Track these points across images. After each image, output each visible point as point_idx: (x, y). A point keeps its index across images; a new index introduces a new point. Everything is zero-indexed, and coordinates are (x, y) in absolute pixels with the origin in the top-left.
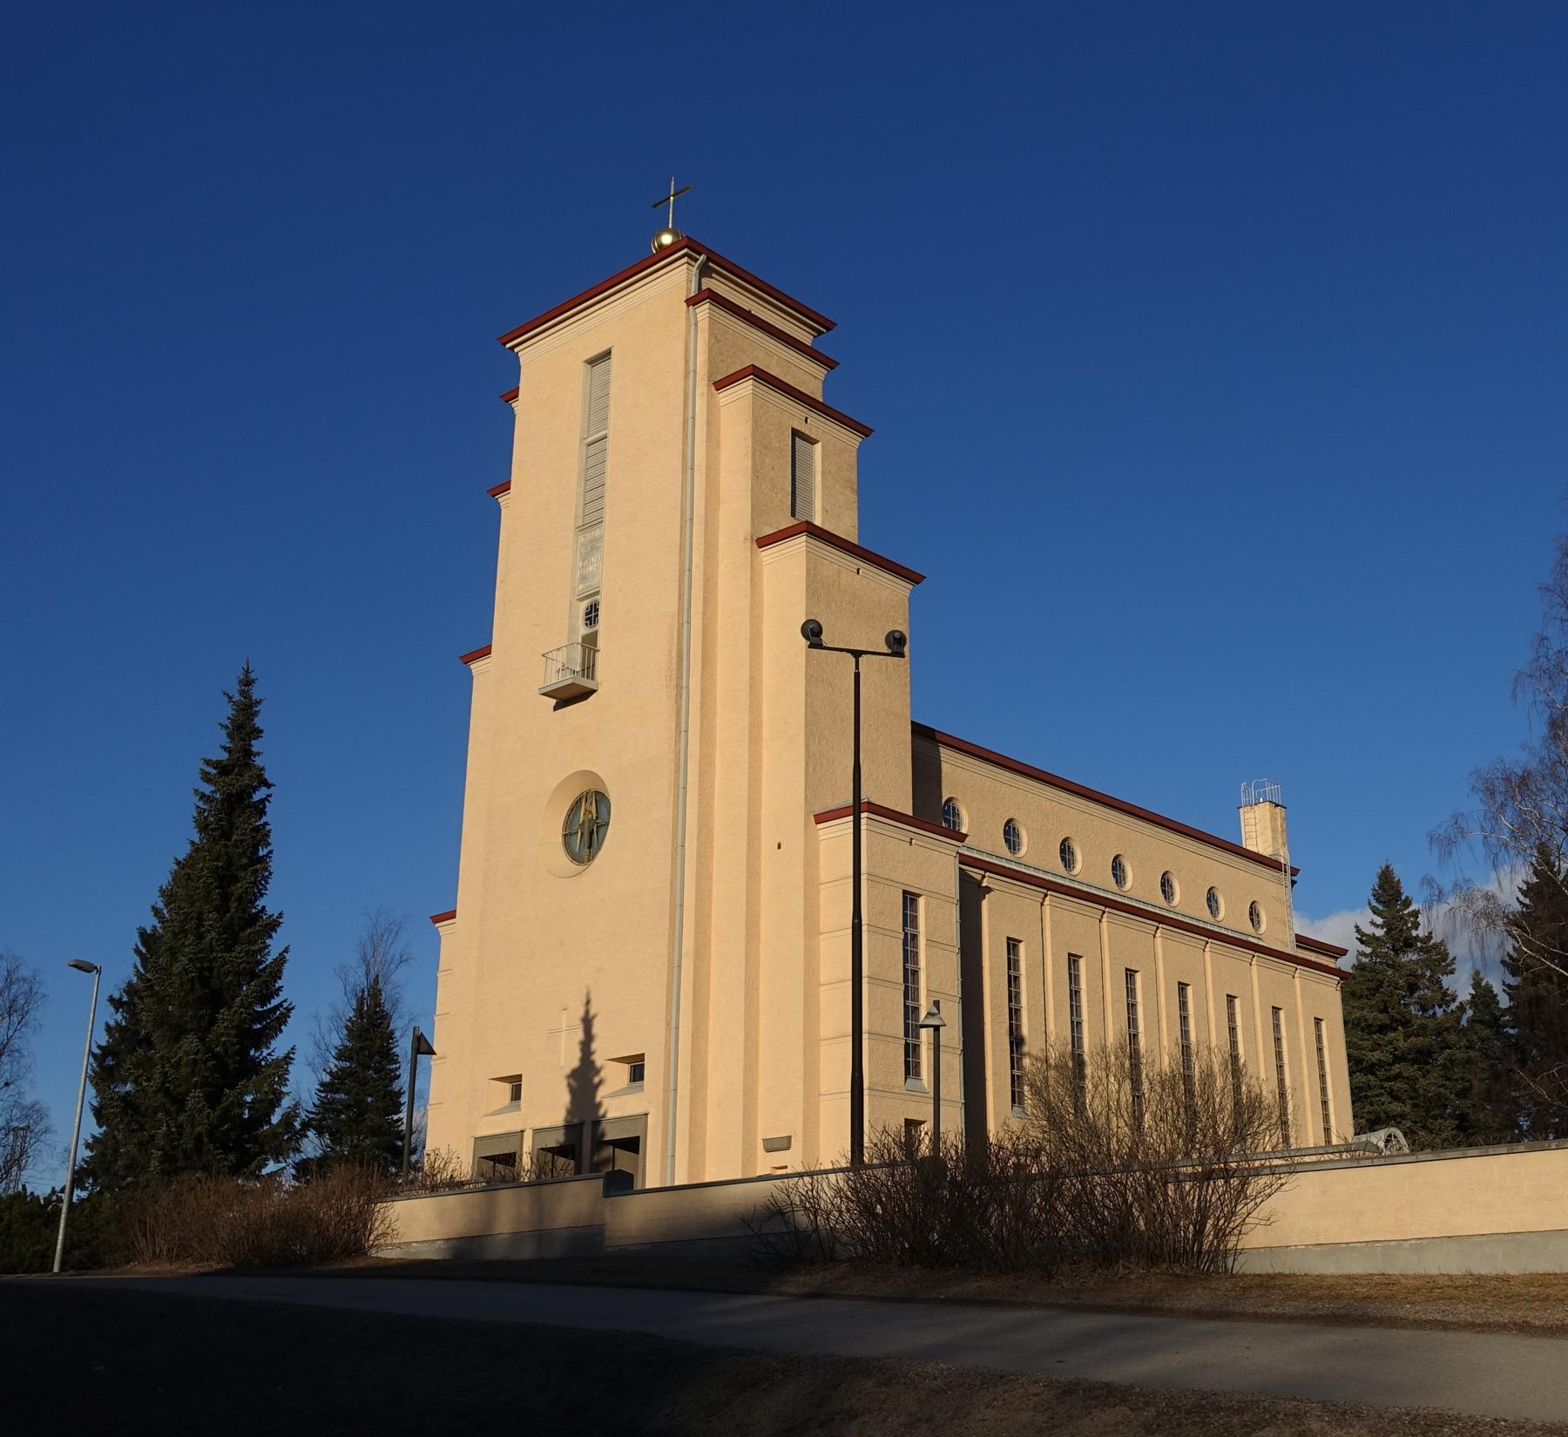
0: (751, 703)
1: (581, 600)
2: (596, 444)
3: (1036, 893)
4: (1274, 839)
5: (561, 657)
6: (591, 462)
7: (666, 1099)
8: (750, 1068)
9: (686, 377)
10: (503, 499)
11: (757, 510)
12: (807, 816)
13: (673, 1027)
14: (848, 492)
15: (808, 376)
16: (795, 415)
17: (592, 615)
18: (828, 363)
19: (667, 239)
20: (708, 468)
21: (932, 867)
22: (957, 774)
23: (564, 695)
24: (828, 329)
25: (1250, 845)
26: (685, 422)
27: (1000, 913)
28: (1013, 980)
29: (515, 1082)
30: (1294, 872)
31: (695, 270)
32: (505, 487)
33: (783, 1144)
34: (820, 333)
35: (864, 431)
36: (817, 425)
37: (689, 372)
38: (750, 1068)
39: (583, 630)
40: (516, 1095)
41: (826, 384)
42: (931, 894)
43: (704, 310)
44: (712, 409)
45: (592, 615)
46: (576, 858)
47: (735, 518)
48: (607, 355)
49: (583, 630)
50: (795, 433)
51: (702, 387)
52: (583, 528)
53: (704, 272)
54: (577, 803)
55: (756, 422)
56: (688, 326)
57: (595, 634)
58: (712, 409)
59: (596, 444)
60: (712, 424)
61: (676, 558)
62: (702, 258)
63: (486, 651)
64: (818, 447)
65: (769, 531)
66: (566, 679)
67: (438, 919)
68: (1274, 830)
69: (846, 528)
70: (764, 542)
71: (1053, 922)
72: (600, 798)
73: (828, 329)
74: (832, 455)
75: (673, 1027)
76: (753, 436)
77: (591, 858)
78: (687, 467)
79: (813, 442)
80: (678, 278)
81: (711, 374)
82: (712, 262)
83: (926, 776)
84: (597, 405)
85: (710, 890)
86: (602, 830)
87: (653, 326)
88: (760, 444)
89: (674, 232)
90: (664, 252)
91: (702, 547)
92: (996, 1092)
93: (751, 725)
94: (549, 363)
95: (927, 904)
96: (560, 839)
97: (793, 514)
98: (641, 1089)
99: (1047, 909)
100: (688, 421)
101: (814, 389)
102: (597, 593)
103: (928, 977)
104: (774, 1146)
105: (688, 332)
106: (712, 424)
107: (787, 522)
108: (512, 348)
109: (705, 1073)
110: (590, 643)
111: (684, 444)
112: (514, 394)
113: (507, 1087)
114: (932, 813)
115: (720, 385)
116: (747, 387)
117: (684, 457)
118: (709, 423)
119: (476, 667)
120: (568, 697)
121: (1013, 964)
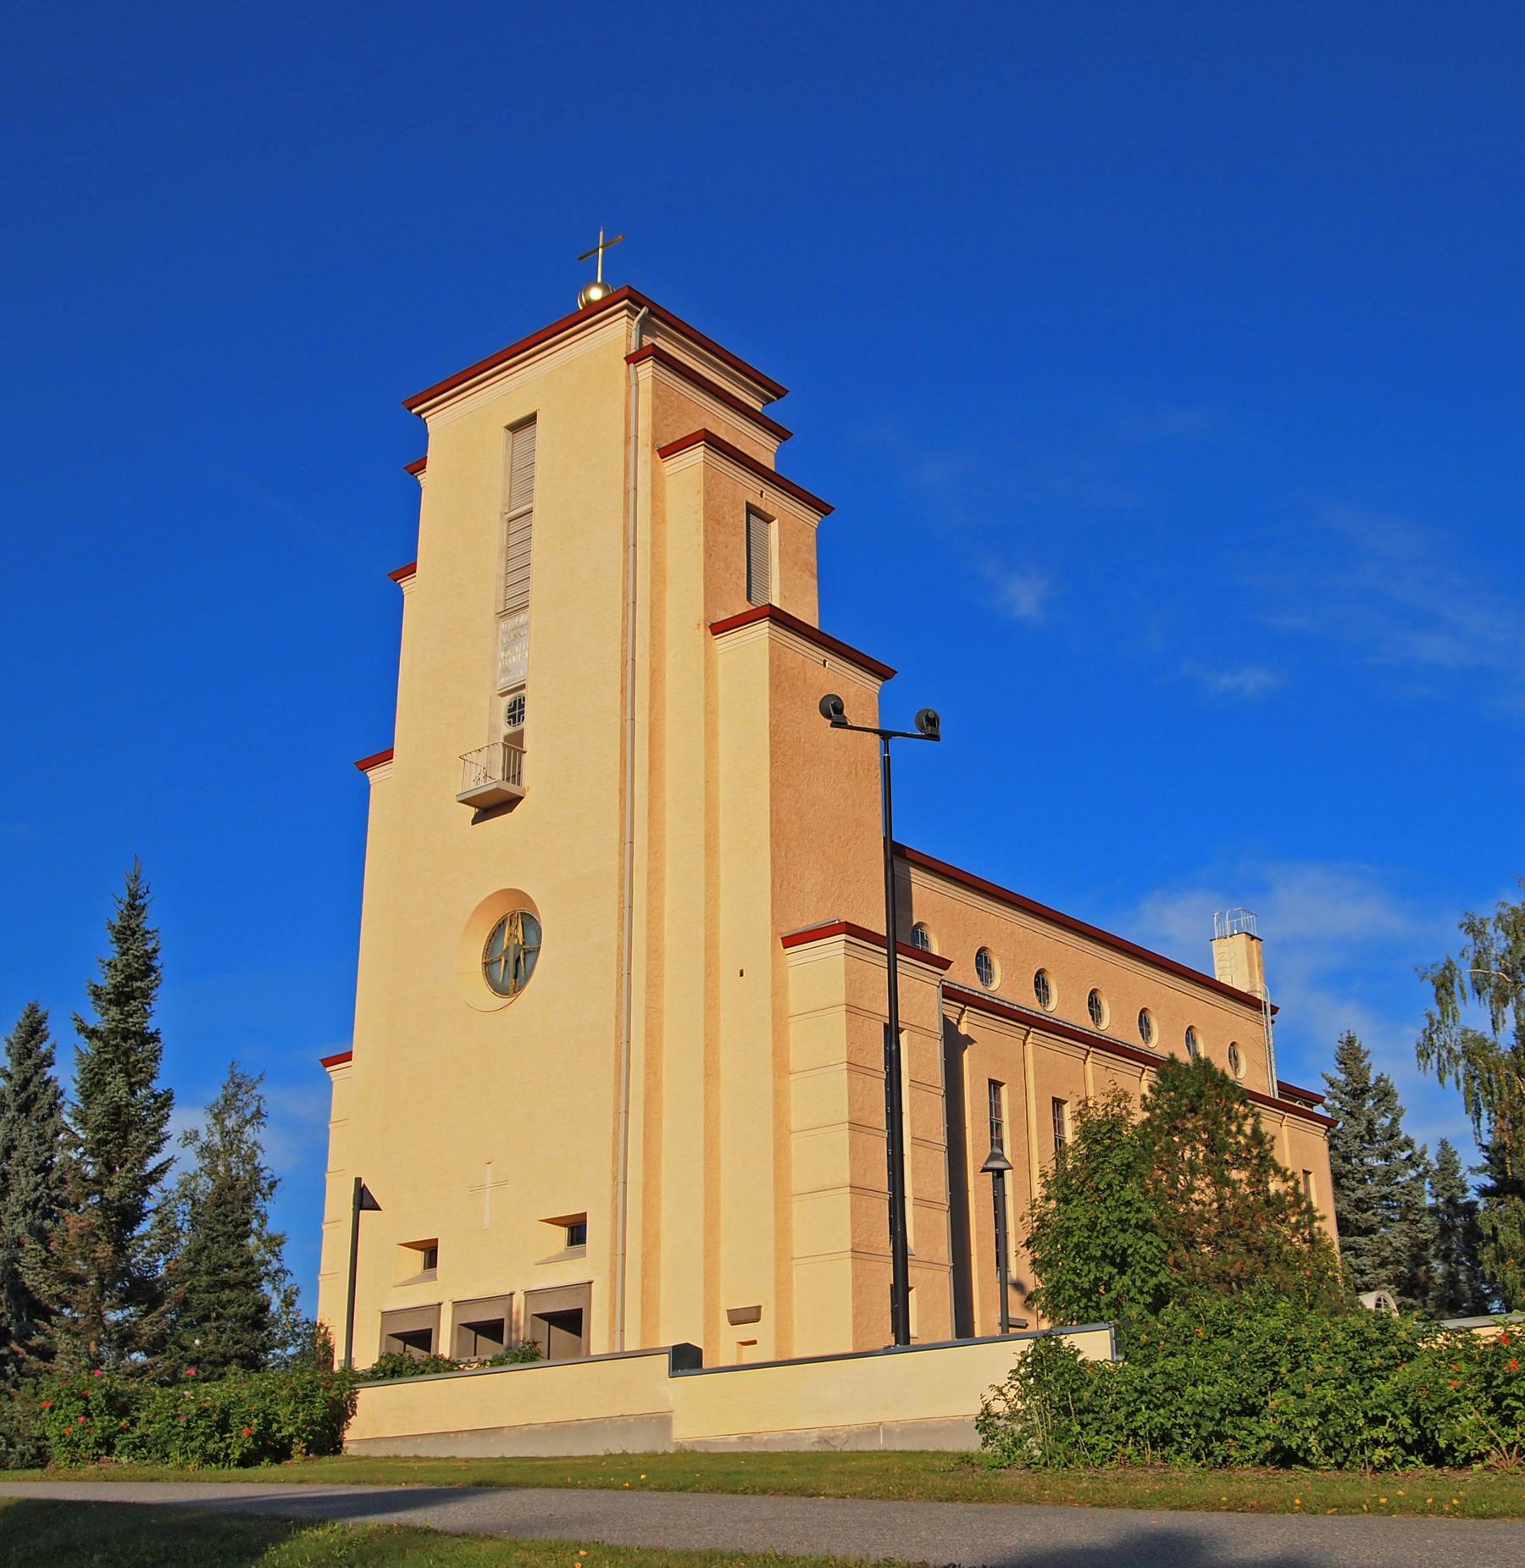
0: (707, 810)
1: (503, 695)
2: (519, 519)
3: (1018, 1030)
4: (1251, 974)
5: (482, 759)
6: (514, 539)
7: (613, 1264)
8: (711, 1228)
9: (627, 443)
10: (407, 585)
11: (712, 591)
12: (774, 936)
13: (621, 1181)
14: (806, 576)
15: (763, 448)
16: (752, 490)
17: (516, 712)
18: (781, 433)
19: (596, 294)
20: (654, 545)
21: (921, 997)
22: (924, 889)
23: (488, 802)
24: (779, 397)
25: (1222, 976)
26: (626, 493)
27: (991, 1048)
28: (996, 1127)
29: (430, 1251)
30: (1274, 1010)
31: (635, 323)
32: (410, 569)
33: (751, 1315)
34: (769, 401)
35: (823, 508)
36: (773, 500)
37: (630, 438)
38: (711, 1228)
39: (506, 729)
40: (431, 1261)
41: (778, 457)
42: (916, 1029)
43: (647, 368)
44: (656, 479)
45: (516, 712)
46: (500, 990)
47: (686, 601)
48: (531, 420)
49: (506, 729)
50: (751, 510)
51: (645, 454)
52: (505, 614)
53: (645, 327)
54: (500, 926)
55: (709, 495)
56: (629, 386)
57: (521, 732)
58: (656, 479)
59: (519, 519)
60: (657, 496)
61: (617, 646)
62: (644, 310)
63: (387, 756)
64: (775, 525)
65: (723, 616)
66: (486, 786)
67: (328, 1062)
68: (1251, 966)
69: (808, 612)
70: (719, 628)
71: (1036, 1062)
72: (529, 921)
73: (779, 397)
74: (790, 532)
75: (621, 1181)
76: (706, 511)
77: (518, 989)
78: (630, 545)
79: (768, 519)
80: (618, 332)
81: (655, 439)
82: (656, 317)
83: (898, 899)
84: (521, 477)
85: (661, 1025)
86: (530, 958)
87: (590, 383)
88: (713, 518)
89: (604, 286)
90: (593, 308)
91: (647, 634)
92: (980, 1254)
93: (707, 836)
94: (462, 433)
95: (910, 1039)
96: (479, 968)
97: (749, 599)
98: (583, 1254)
99: (1029, 1047)
100: (630, 492)
101: (768, 460)
102: (523, 687)
103: (912, 1122)
104: (742, 1317)
105: (628, 393)
106: (657, 496)
107: (742, 607)
108: (419, 414)
109: (657, 1236)
110: (514, 745)
111: (626, 517)
112: (421, 465)
113: (421, 1254)
114: (902, 940)
115: (666, 452)
116: (697, 454)
117: (625, 533)
118: (654, 495)
119: (374, 775)
120: (492, 806)
121: (995, 1109)
